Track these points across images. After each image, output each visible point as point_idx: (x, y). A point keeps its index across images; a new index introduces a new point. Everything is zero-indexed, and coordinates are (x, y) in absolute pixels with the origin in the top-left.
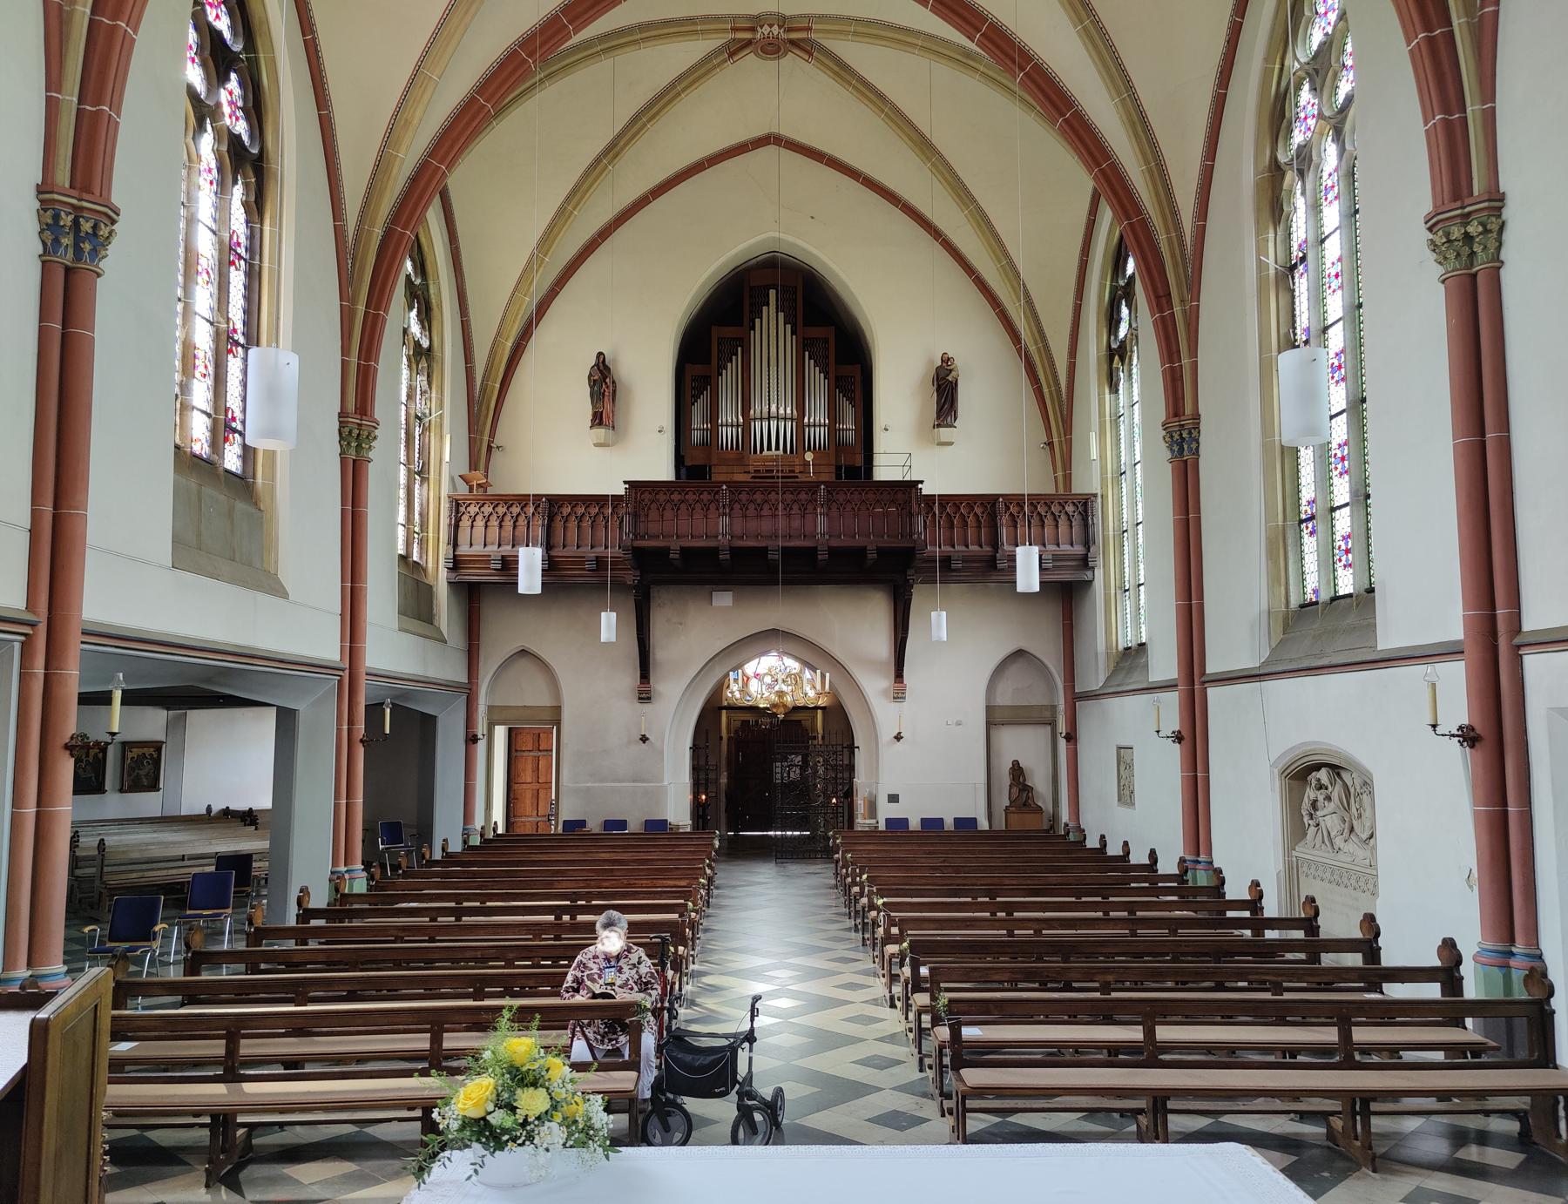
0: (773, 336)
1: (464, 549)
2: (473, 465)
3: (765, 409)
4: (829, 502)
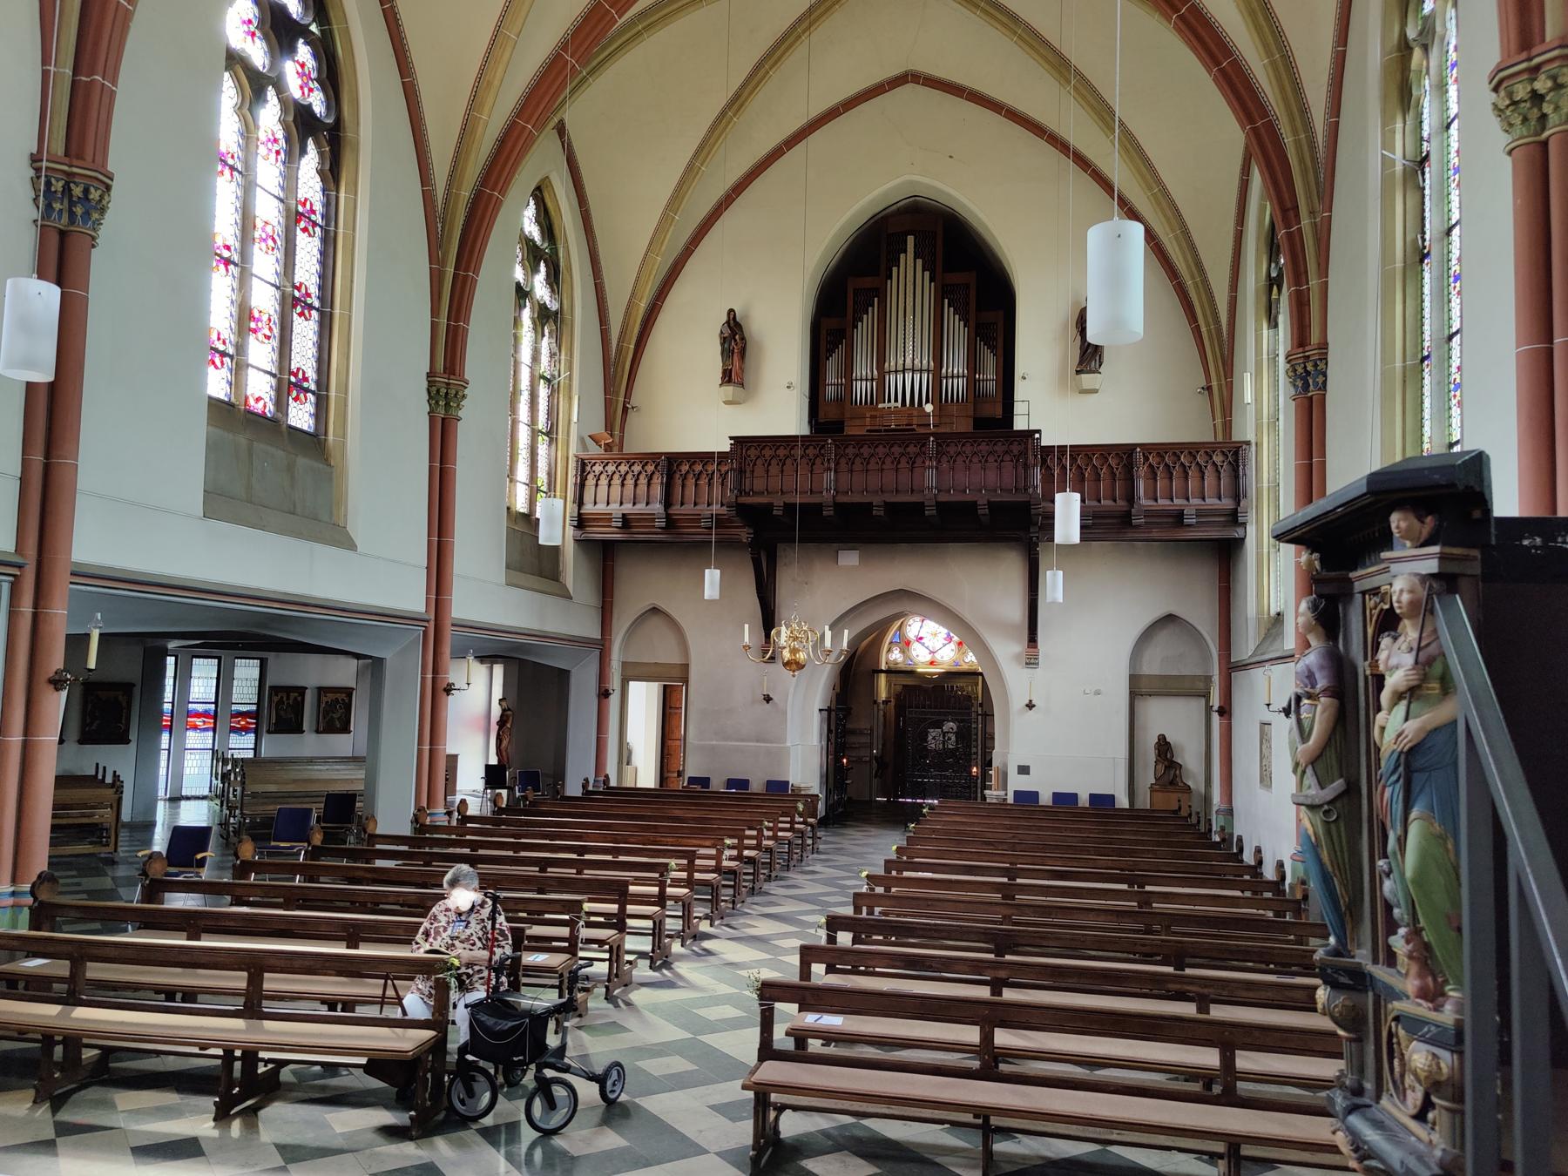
0: (911, 284)
1: (588, 508)
2: (609, 426)
3: (900, 362)
4: (940, 454)
